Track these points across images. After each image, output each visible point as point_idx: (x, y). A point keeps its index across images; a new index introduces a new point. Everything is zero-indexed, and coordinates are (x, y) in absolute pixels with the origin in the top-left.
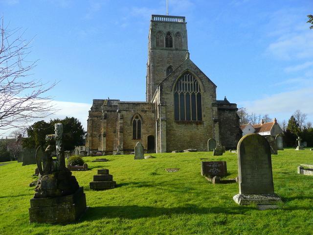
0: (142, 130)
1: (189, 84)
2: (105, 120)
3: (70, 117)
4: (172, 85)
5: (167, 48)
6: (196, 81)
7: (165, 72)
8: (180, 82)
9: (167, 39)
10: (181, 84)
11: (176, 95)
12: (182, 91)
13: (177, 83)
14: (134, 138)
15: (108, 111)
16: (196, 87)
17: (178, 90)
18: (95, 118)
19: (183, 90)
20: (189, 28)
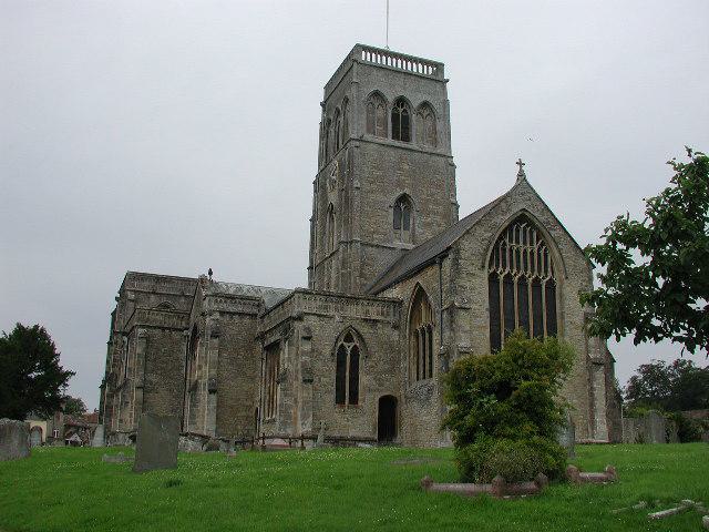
0: (364, 380)
1: (525, 252)
2: (216, 341)
3: (29, 324)
4: (488, 249)
5: (397, 143)
6: (542, 245)
7: (391, 211)
8: (505, 244)
9: (395, 117)
10: (504, 250)
11: (493, 278)
12: (536, 273)
13: (496, 247)
14: (340, 400)
15: (222, 313)
16: (544, 262)
17: (497, 266)
18: (156, 332)
19: (539, 271)
20: (457, 95)
